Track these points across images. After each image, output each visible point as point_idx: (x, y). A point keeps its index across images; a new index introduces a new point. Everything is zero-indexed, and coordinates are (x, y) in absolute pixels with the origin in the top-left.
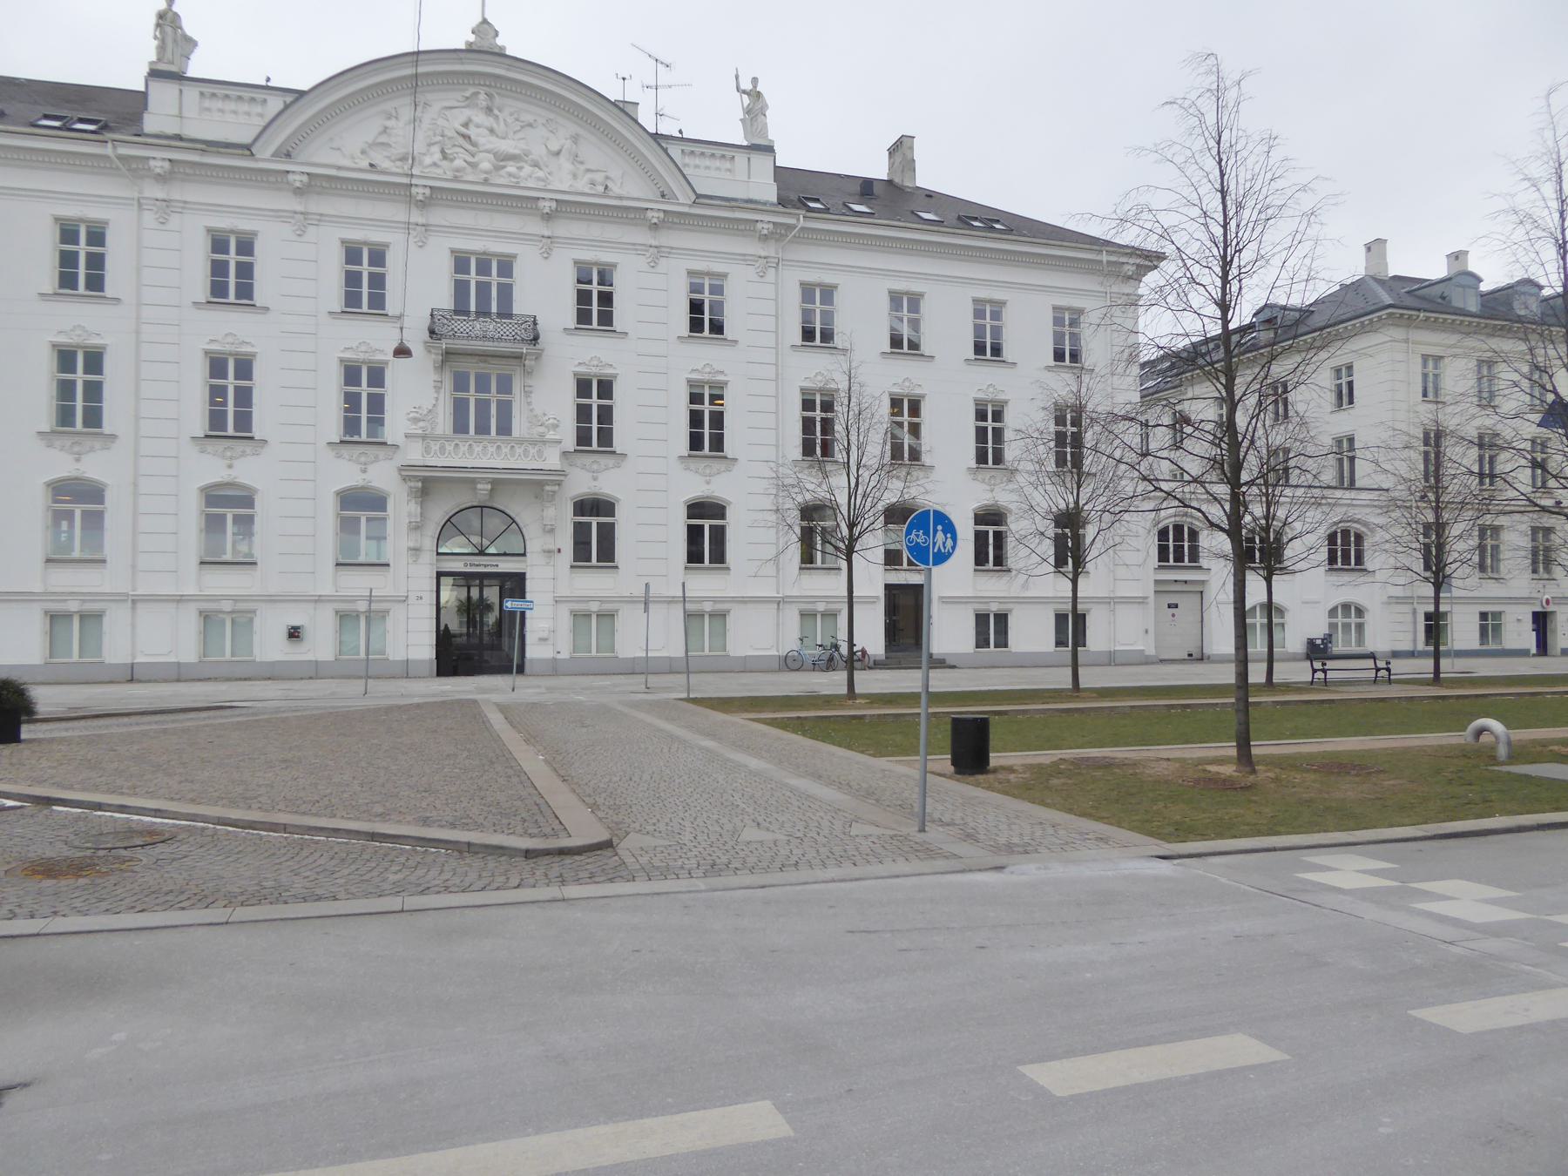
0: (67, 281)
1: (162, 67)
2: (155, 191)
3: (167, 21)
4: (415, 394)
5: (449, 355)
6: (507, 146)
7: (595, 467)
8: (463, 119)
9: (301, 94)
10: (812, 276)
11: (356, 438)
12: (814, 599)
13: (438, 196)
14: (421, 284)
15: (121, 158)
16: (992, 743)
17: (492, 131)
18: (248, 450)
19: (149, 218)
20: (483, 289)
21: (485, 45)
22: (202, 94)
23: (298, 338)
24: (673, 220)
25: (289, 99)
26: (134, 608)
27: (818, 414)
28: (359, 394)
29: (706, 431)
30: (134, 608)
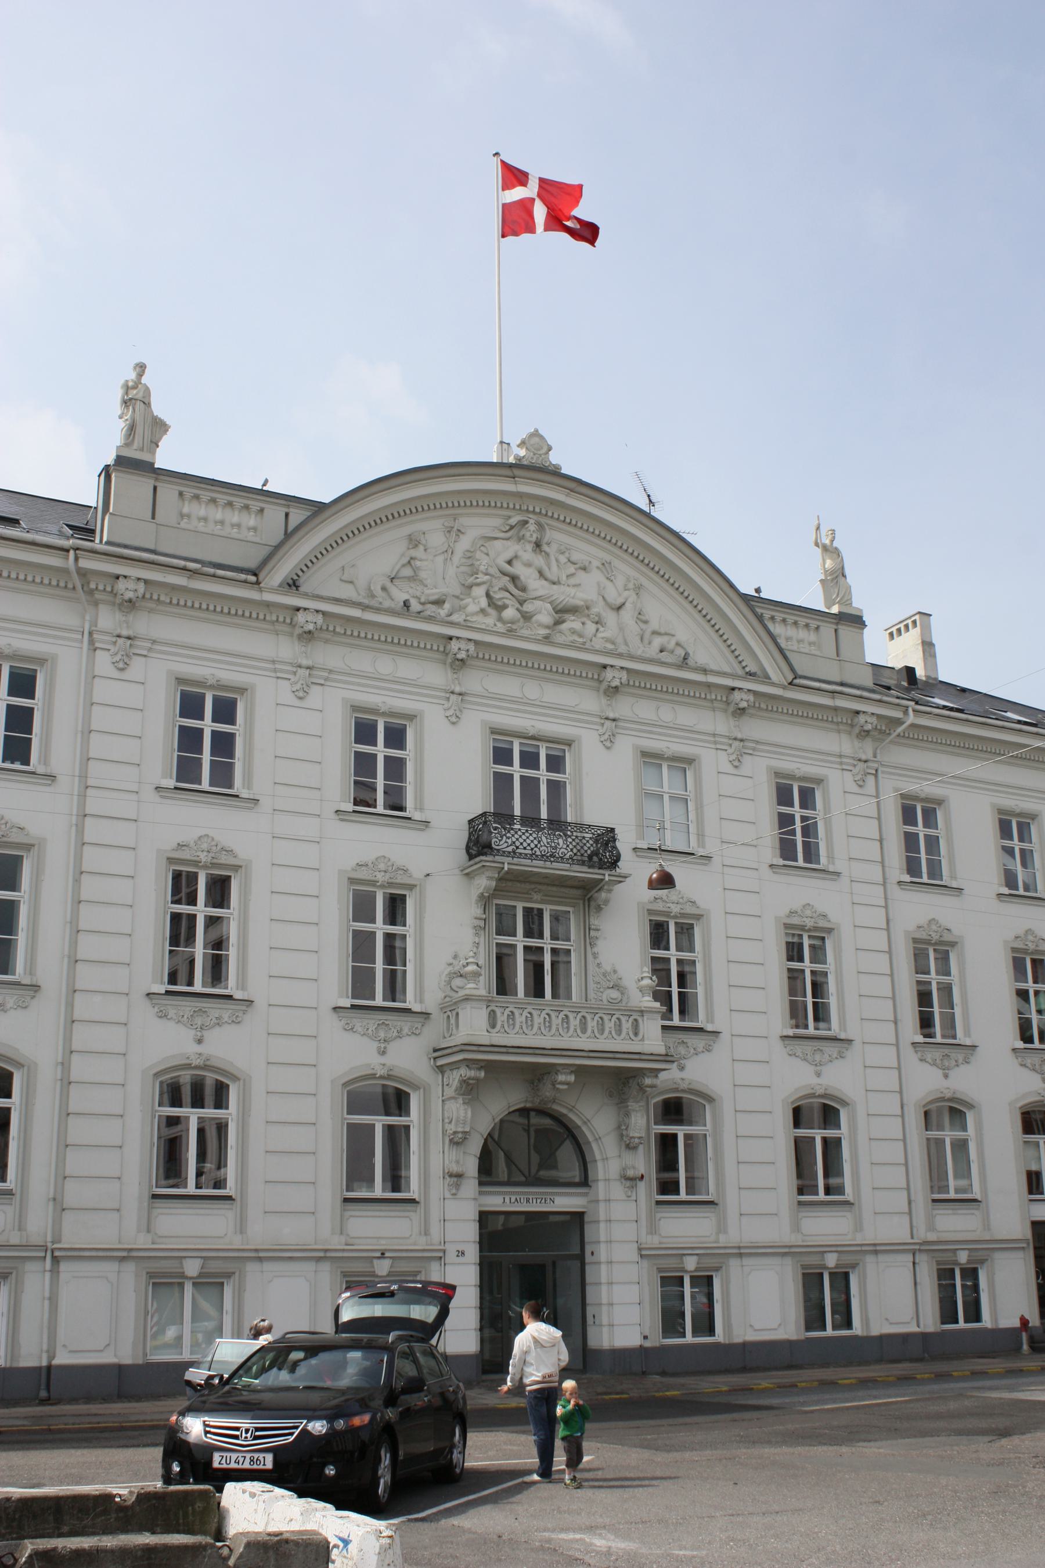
2: (107, 619)
3: (135, 397)
4: (448, 934)
5: (510, 883)
6: (565, 595)
7: (818, 1057)
8: (508, 555)
9: (318, 509)
10: (912, 787)
11: (801, 1031)
12: (822, 1250)
14: (451, 778)
15: (83, 573)
16: (555, 1453)
17: (541, 574)
19: (103, 662)
20: (530, 786)
21: (536, 461)
22: (181, 494)
23: (295, 853)
24: (768, 705)
25: (297, 516)
26: (55, 1271)
29: (809, 1002)
30: (55, 1271)
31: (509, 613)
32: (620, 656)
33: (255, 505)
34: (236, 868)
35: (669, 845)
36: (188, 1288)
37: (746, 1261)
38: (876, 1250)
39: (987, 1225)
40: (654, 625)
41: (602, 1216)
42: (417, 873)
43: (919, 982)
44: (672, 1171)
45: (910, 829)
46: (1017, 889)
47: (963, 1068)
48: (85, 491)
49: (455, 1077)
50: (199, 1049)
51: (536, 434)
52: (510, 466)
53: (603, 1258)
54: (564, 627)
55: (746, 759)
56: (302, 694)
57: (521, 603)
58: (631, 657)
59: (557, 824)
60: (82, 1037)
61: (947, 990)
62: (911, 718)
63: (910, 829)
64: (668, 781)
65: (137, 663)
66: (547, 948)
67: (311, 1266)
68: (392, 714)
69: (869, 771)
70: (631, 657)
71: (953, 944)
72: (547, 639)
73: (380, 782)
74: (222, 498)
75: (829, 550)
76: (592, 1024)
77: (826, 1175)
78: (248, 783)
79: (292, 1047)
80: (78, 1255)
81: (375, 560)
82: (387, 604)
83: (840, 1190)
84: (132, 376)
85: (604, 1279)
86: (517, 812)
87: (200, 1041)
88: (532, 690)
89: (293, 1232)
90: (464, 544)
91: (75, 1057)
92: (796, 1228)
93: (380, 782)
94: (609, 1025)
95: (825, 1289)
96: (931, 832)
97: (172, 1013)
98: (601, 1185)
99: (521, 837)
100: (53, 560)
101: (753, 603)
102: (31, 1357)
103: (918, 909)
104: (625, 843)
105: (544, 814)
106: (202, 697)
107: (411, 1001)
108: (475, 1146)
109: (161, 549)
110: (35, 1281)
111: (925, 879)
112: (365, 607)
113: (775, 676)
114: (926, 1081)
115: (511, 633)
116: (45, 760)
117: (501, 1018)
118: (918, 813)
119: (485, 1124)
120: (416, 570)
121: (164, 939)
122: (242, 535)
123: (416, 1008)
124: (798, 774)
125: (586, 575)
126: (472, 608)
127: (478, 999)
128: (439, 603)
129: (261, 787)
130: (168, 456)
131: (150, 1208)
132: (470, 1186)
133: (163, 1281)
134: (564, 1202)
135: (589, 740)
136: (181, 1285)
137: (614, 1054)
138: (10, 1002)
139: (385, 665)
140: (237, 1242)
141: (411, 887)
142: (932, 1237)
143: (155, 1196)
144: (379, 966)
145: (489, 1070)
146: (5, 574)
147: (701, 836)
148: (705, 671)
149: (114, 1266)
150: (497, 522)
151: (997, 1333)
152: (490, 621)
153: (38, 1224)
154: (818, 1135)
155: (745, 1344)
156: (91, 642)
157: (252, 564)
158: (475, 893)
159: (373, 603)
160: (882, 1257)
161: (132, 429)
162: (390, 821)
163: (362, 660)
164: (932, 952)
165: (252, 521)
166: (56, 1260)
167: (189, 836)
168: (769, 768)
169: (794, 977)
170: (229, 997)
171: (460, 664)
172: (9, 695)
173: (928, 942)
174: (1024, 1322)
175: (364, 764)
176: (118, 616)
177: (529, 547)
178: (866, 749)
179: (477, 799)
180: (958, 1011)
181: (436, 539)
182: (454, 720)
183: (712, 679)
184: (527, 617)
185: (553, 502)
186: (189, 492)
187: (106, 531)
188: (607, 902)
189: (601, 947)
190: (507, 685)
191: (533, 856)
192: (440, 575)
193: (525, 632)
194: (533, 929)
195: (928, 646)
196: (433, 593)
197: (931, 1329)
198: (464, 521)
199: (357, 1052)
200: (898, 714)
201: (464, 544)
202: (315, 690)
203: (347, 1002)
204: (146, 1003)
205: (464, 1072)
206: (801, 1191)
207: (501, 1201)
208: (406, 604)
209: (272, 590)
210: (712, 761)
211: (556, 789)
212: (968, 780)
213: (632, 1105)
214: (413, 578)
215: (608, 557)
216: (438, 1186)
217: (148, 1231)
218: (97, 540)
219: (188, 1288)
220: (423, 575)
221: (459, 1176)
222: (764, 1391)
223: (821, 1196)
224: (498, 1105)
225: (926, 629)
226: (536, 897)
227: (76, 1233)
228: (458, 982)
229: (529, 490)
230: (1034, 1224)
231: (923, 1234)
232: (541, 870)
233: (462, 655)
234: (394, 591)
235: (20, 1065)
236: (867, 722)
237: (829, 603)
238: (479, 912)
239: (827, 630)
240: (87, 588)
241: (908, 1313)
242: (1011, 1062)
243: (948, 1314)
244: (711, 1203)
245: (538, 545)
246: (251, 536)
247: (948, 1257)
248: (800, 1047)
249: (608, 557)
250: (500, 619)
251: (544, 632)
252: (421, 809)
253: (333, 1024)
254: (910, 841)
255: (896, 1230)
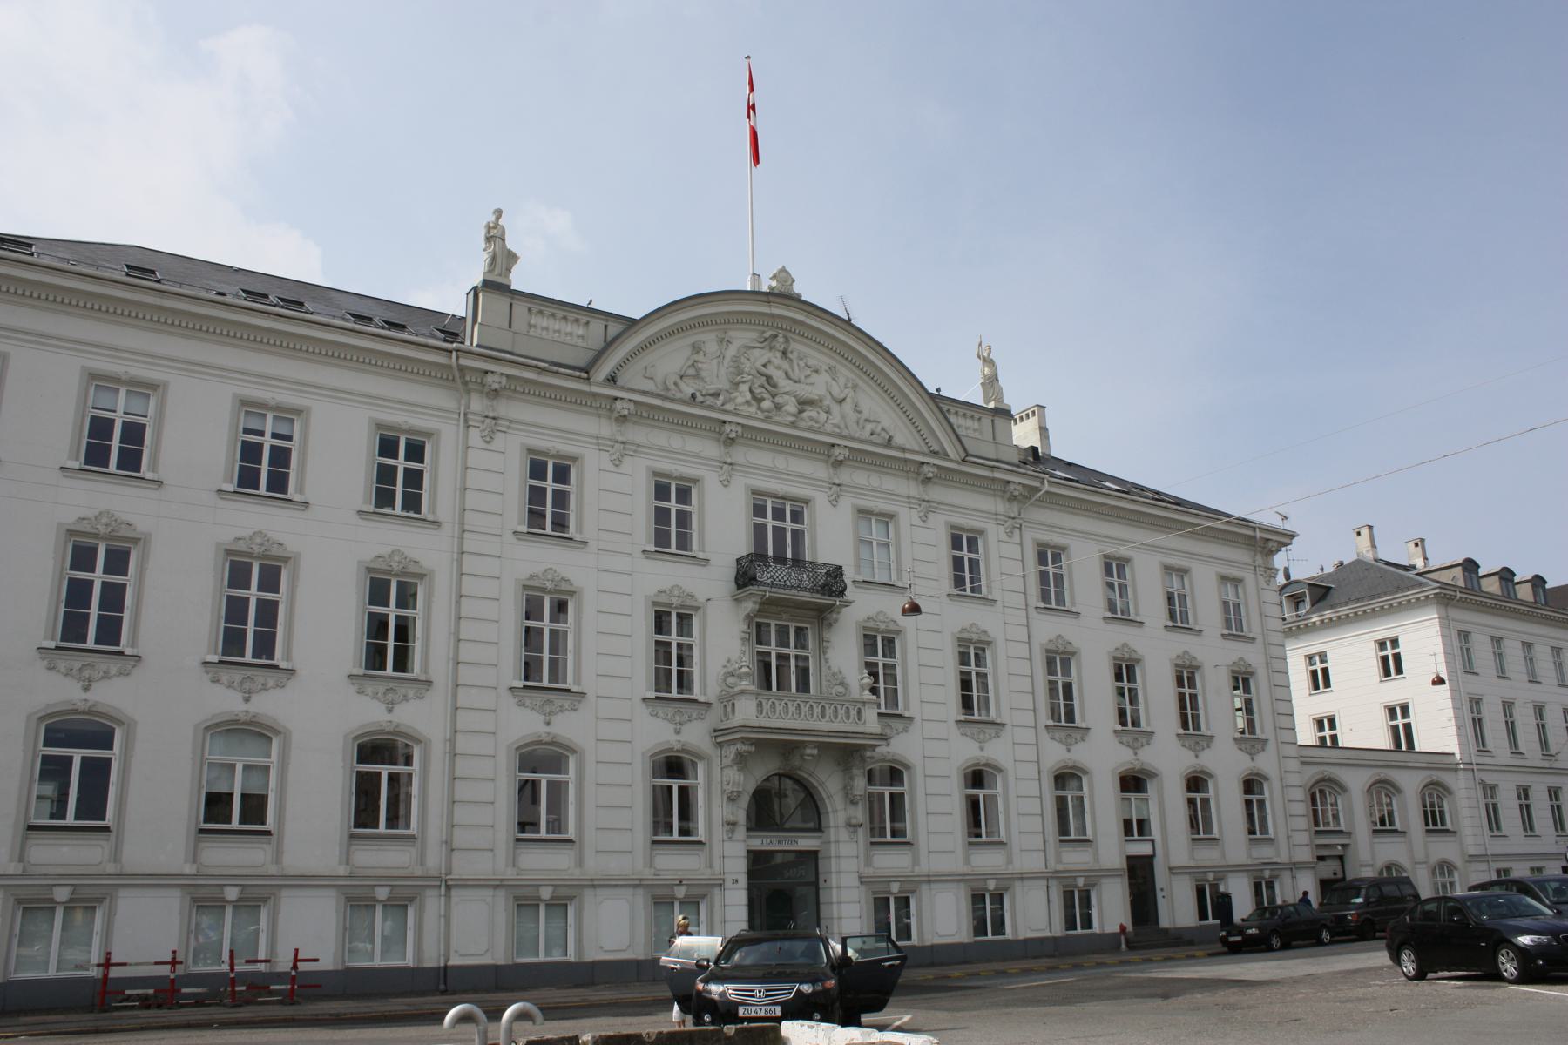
0: (384, 498)
1: (492, 278)
2: (477, 404)
4: (721, 644)
5: (769, 606)
6: (805, 391)
8: (764, 360)
9: (631, 323)
10: (1046, 537)
12: (985, 878)
13: (754, 436)
14: (724, 529)
15: (462, 369)
18: (114, 669)
19: (475, 436)
20: (779, 533)
23: (614, 580)
24: (947, 476)
25: (614, 329)
26: (448, 896)
27: (392, 611)
28: (247, 600)
29: (541, 664)
31: (767, 404)
32: (844, 437)
33: (583, 319)
34: (572, 593)
35: (877, 579)
36: (229, 911)
37: (934, 886)
38: (1022, 877)
39: (1096, 859)
40: (866, 414)
41: (833, 853)
42: (701, 598)
43: (962, 673)
44: (889, 820)
45: (958, 553)
46: (669, 546)
47: (1207, 751)
48: (454, 303)
49: (731, 752)
50: (547, 729)
51: (783, 270)
52: (766, 294)
53: (834, 883)
54: (805, 415)
55: (931, 516)
56: (617, 463)
57: (774, 396)
58: (853, 439)
59: (798, 562)
60: (464, 720)
61: (982, 677)
62: (1046, 487)
63: (958, 553)
64: (876, 531)
65: (499, 437)
66: (793, 655)
67: (630, 891)
68: (681, 478)
69: (1015, 525)
70: (853, 439)
71: (1073, 654)
72: (793, 425)
73: (549, 510)
74: (560, 313)
75: (988, 361)
76: (829, 712)
77: (892, 820)
78: (580, 529)
79: (614, 729)
80: (465, 884)
81: (669, 361)
82: (679, 395)
83: (903, 833)
84: (493, 218)
85: (835, 899)
86: (770, 553)
87: (548, 724)
88: (781, 462)
89: (615, 866)
90: (731, 352)
91: (459, 736)
92: (967, 861)
93: (549, 510)
94: (842, 712)
95: (986, 904)
96: (973, 556)
97: (528, 703)
98: (832, 831)
99: (777, 572)
100: (440, 359)
101: (936, 399)
102: (432, 960)
103: (1049, 628)
104: (849, 575)
105: (789, 555)
106: (545, 463)
107: (697, 693)
108: (745, 801)
109: (517, 351)
110: (433, 903)
111: (1054, 606)
112: (665, 398)
113: (952, 454)
114: (1056, 754)
115: (767, 419)
116: (433, 509)
117: (766, 707)
118: (1048, 554)
119: (751, 788)
120: (698, 370)
121: (219, 617)
122: (577, 340)
123: (702, 699)
124: (676, 474)
125: (816, 376)
126: (740, 400)
127: (750, 693)
128: (716, 395)
129: (589, 533)
130: (520, 280)
131: (197, 842)
132: (741, 832)
133: (525, 903)
134: (806, 843)
135: (820, 499)
136: (53, 909)
137: (845, 734)
138: (411, 693)
139: (676, 441)
140: (577, 874)
141: (697, 609)
142: (1059, 867)
143: (202, 831)
144: (391, 643)
145: (761, 744)
146: (4, 288)
147: (900, 570)
148: (904, 450)
149: (490, 892)
150: (755, 335)
151: (1102, 936)
152: (753, 410)
153: (434, 860)
154: (887, 791)
155: (932, 946)
156: (466, 420)
157: (582, 363)
158: (742, 615)
159: (669, 395)
160: (1026, 883)
161: (493, 259)
162: (268, 502)
163: (660, 438)
164: (1058, 659)
165: (581, 331)
166: (448, 888)
167: (538, 569)
168: (947, 523)
169: (662, 649)
170: (568, 691)
171: (730, 442)
172: (380, 455)
173: (1056, 652)
174: (1123, 928)
175: (536, 495)
176: (486, 401)
177: (778, 355)
178: (1014, 510)
179: (742, 545)
180: (991, 695)
181: (712, 347)
182: (726, 483)
183: (908, 456)
184: (778, 407)
185: (795, 321)
186: (535, 308)
187: (473, 338)
188: (836, 621)
189: (831, 654)
190: (763, 458)
191: (785, 587)
192: (716, 375)
193: (777, 419)
194: (801, 644)
195: (1043, 431)
196: (712, 388)
197: (1059, 934)
198: (731, 333)
199: (659, 732)
200: (1036, 484)
201: (731, 352)
202: (627, 460)
203: (653, 695)
204: (508, 695)
205: (740, 747)
206: (523, 826)
207: (761, 842)
208: (693, 396)
209: (598, 384)
210: (907, 517)
211: (797, 536)
212: (152, 356)
213: (855, 771)
214: (697, 376)
215: (833, 363)
216: (719, 832)
217: (194, 861)
218: (468, 343)
219: (229, 911)
220: (703, 374)
221: (734, 824)
222: (959, 978)
223: (889, 838)
224: (761, 771)
225: (1042, 419)
226: (785, 616)
227: (464, 867)
228: (731, 680)
229: (778, 312)
230: (1129, 858)
231: (1053, 865)
232: (790, 596)
233: (733, 435)
234: (683, 385)
235: (120, 723)
236: (1018, 490)
237: (987, 401)
238: (745, 627)
239: (987, 421)
240: (462, 380)
241: (1043, 924)
242: (1112, 741)
243: (1070, 923)
244: (908, 843)
245: (784, 353)
246: (580, 342)
247: (1070, 881)
248: (969, 729)
249: (833, 363)
250: (759, 408)
251: (791, 419)
252: (154, 471)
253: (643, 711)
254: (1044, 577)
255: (1034, 863)
